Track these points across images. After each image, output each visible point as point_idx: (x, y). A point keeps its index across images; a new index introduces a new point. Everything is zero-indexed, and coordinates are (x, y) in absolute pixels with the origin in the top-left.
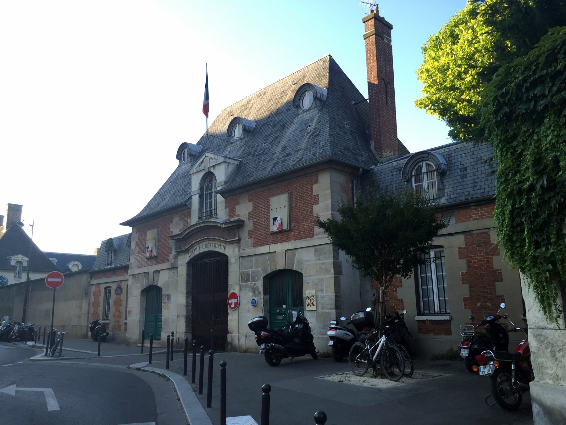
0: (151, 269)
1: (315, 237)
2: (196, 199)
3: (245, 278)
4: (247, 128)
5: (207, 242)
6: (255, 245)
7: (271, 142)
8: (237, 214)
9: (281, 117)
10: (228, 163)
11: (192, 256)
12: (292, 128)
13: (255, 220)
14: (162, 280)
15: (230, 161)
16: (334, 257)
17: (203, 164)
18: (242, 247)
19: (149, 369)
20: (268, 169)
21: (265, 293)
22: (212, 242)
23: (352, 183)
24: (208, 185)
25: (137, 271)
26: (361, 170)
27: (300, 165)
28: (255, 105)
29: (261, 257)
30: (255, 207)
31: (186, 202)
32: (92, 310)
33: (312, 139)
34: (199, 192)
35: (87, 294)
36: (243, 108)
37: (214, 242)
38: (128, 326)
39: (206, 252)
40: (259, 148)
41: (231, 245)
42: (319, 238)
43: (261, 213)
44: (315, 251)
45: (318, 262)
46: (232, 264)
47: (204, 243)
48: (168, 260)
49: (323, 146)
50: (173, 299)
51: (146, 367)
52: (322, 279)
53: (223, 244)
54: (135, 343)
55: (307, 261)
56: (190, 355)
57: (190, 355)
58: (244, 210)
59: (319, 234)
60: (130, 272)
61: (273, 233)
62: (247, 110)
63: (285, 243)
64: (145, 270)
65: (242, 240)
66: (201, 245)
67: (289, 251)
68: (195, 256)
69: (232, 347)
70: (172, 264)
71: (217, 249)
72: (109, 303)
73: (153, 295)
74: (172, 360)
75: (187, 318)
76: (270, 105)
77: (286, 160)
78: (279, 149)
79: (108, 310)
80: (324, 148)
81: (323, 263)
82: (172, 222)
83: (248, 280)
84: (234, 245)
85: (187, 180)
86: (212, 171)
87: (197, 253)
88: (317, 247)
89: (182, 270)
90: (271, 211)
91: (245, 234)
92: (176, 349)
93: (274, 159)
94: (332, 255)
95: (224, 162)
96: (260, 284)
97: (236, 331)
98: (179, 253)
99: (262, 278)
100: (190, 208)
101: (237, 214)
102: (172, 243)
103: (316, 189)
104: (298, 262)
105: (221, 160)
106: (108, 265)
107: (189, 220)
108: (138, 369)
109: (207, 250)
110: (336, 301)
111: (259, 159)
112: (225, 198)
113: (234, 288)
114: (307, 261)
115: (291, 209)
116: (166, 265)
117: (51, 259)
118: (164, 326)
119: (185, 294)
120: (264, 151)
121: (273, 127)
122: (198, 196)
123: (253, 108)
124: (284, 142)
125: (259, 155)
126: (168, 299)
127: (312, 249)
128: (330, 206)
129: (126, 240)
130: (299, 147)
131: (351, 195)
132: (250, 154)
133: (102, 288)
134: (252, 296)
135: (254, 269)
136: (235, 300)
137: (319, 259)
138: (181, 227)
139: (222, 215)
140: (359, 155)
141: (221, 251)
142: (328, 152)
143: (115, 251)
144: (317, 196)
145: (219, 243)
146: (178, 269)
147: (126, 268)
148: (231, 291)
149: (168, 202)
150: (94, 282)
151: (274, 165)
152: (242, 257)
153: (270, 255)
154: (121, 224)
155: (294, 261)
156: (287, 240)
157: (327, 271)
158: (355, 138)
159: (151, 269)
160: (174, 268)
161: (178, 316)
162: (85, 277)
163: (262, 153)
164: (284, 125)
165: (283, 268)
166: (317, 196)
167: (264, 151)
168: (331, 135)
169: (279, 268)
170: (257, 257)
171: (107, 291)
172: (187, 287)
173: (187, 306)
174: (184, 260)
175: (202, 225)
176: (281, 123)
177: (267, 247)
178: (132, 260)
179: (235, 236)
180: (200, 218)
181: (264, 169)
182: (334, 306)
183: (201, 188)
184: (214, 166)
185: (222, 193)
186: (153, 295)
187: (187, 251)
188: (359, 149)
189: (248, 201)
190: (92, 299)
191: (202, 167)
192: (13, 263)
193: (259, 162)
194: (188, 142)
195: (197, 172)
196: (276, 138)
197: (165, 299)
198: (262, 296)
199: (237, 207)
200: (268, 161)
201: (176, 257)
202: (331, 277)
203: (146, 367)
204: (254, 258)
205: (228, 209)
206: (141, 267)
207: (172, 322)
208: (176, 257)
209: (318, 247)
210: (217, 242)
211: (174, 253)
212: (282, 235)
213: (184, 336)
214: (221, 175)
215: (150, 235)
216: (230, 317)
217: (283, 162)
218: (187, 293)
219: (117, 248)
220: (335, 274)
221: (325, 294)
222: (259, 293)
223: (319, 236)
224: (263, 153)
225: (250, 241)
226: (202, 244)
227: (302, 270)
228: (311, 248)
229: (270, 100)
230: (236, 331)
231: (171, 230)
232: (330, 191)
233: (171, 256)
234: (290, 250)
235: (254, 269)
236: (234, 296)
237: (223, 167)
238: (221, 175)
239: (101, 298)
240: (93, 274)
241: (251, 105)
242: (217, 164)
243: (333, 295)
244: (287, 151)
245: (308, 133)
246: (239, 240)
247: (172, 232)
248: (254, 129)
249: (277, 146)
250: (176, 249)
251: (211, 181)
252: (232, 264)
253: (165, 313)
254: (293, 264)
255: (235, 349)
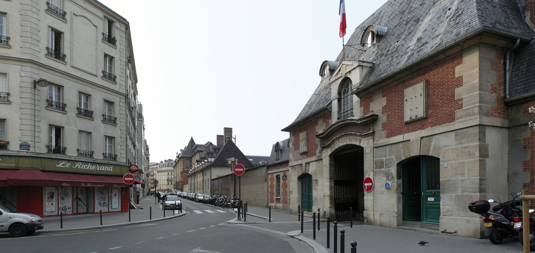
0: (304, 162)
1: (456, 121)
2: (335, 103)
3: (379, 165)
4: (379, 33)
5: (345, 138)
6: (388, 136)
7: (404, 39)
8: (371, 110)
9: (414, 14)
10: (363, 66)
11: (333, 150)
12: (427, 20)
13: (388, 113)
14: (312, 169)
15: (365, 64)
16: (480, 140)
17: (341, 72)
18: (376, 139)
19: (300, 238)
20: (403, 63)
21: (398, 177)
22: (349, 137)
23: (505, 59)
24: (345, 90)
25: (295, 163)
26: (519, 41)
27: (440, 48)
28: (386, 13)
29: (394, 147)
30: (388, 101)
31: (327, 106)
32: (270, 190)
33: (453, 20)
34: (337, 96)
35: (266, 180)
36: (374, 20)
37: (351, 137)
38: (291, 201)
39: (344, 145)
40: (391, 48)
41: (366, 138)
42: (461, 122)
43: (396, 107)
44: (455, 136)
45: (459, 146)
46: (367, 154)
47: (343, 139)
48: (315, 154)
49: (469, 23)
50: (320, 182)
51: (299, 235)
52: (464, 163)
53: (359, 138)
54: (295, 213)
55: (445, 146)
56: (332, 225)
57: (332, 225)
58: (378, 106)
59: (462, 117)
60: (290, 164)
61: (407, 123)
62: (379, 20)
63: (420, 131)
64: (299, 162)
65: (376, 133)
66: (340, 140)
67: (425, 138)
68: (336, 150)
69: (367, 221)
70: (318, 157)
71: (354, 143)
72: (279, 185)
73: (306, 179)
74: (319, 229)
75: (331, 197)
76: (402, 7)
77: (422, 49)
78: (415, 40)
79: (279, 190)
80: (472, 22)
81: (465, 147)
82: (317, 125)
83: (382, 167)
84: (369, 137)
85: (328, 91)
86: (349, 76)
87: (337, 147)
88: (458, 131)
89: (326, 161)
90: (405, 103)
91: (378, 128)
92: (323, 220)
93: (408, 52)
94: (477, 138)
95: (359, 66)
96: (393, 170)
97: (371, 208)
98: (323, 148)
99: (395, 164)
100: (331, 112)
101: (371, 110)
102: (317, 141)
103: (459, 70)
104: (434, 148)
105: (356, 64)
106: (277, 160)
107: (330, 121)
108: (293, 237)
109: (345, 144)
110: (480, 184)
111: (392, 57)
112: (360, 98)
113: (368, 173)
114: (445, 146)
115: (428, 96)
116: (314, 158)
117: (250, 160)
118: (314, 203)
119: (329, 180)
120: (397, 48)
121: (406, 25)
122: (336, 100)
123: (384, 17)
124: (419, 34)
125: (392, 53)
126: (317, 183)
127: (453, 134)
128: (478, 85)
129: (287, 142)
130: (437, 33)
131: (502, 72)
132: (383, 55)
133: (275, 175)
134: (386, 180)
135: (388, 157)
136: (370, 184)
137: (461, 143)
138: (324, 128)
139: (357, 114)
140: (512, 28)
141: (358, 144)
142: (476, 25)
143: (281, 151)
144: (461, 77)
145: (355, 137)
146: (323, 160)
147: (287, 162)
148: (366, 176)
149: (314, 109)
150: (270, 172)
151: (409, 57)
152: (376, 147)
153: (404, 143)
154: (282, 130)
155: (429, 147)
156: (423, 127)
157: (470, 155)
158: (506, 12)
159: (304, 162)
160: (320, 160)
161: (324, 196)
162: (265, 169)
163: (395, 51)
164: (419, 19)
165: (418, 154)
166: (461, 77)
167: (397, 48)
168: (478, 10)
169: (413, 154)
170: (390, 146)
171: (278, 177)
172: (330, 174)
173: (331, 188)
174: (327, 153)
175: (341, 123)
176: (415, 19)
177: (401, 136)
178: (291, 156)
179: (369, 130)
180: (338, 119)
181: (397, 64)
182: (478, 189)
183: (339, 94)
184: (350, 72)
185: (357, 94)
186: (306, 179)
187: (329, 146)
188: (511, 23)
189: (381, 97)
190: (270, 184)
191: (340, 75)
192: (230, 162)
193: (393, 59)
194: (328, 60)
195: (336, 80)
196: (410, 33)
197: (314, 183)
198: (396, 181)
199: (371, 104)
200: (402, 56)
201: (321, 152)
202: (477, 161)
203: (299, 235)
204: (388, 147)
205: (362, 107)
206: (297, 160)
207: (320, 200)
208: (321, 152)
209: (460, 131)
210: (353, 137)
211: (319, 148)
212: (417, 123)
213: (329, 211)
214: (356, 78)
215: (302, 135)
216: (365, 198)
217: (418, 52)
218: (330, 179)
219: (282, 148)
220: (480, 156)
221: (466, 177)
222: (393, 177)
223: (461, 120)
224: (397, 51)
225: (384, 133)
226: (341, 139)
227: (439, 155)
228: (451, 133)
229: (401, 4)
230: (371, 208)
231: (317, 131)
232: (478, 69)
233: (317, 151)
234: (426, 137)
235: (388, 157)
236: (369, 180)
237: (358, 70)
238: (356, 78)
239: (275, 182)
240: (269, 167)
241: (382, 14)
242: (352, 70)
243: (477, 179)
244: (423, 41)
245: (447, 17)
246: (374, 133)
247: (317, 132)
248: (386, 33)
249: (411, 40)
250: (321, 145)
251: (347, 85)
252: (367, 154)
253: (315, 194)
254: (429, 150)
255: (369, 223)
